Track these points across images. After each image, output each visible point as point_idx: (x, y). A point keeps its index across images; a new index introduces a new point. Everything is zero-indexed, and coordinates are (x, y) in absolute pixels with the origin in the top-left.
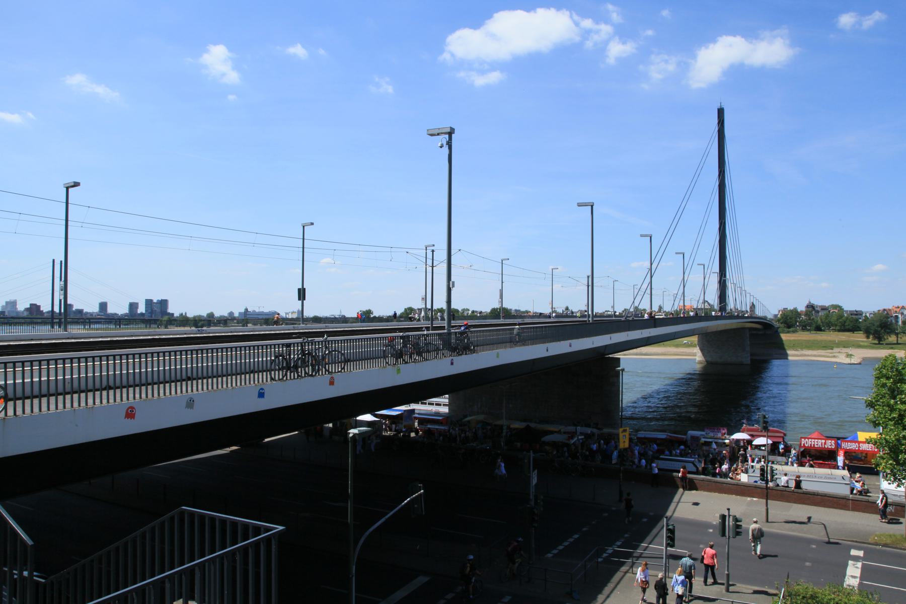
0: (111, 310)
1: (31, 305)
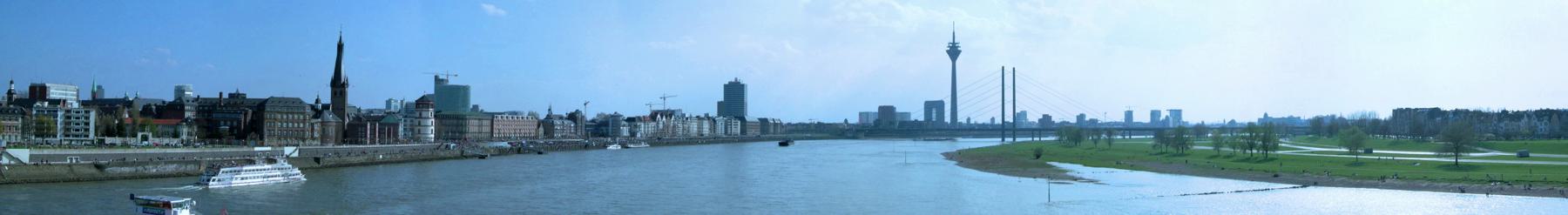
0: (1137, 119)
1: (1044, 116)
